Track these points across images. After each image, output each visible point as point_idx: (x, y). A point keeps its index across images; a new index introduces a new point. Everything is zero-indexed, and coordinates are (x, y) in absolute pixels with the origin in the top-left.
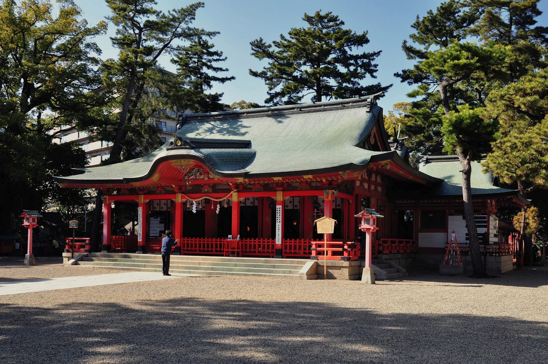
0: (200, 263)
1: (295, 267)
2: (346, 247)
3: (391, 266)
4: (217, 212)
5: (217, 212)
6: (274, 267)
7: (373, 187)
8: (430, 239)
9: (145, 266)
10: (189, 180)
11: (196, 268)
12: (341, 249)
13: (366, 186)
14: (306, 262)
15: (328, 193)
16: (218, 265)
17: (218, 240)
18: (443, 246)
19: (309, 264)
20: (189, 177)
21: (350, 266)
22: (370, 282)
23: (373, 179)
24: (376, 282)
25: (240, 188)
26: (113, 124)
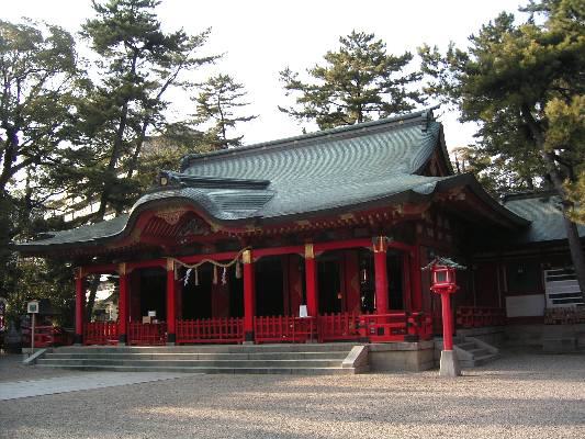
0: (198, 357)
1: (338, 356)
2: (411, 320)
3: (475, 346)
4: (197, 283)
5: (197, 283)
6: (305, 356)
7: (440, 236)
8: (524, 306)
9: (122, 364)
10: (184, 238)
11: (192, 364)
12: (403, 324)
13: (431, 233)
14: (352, 347)
15: (379, 241)
16: (225, 357)
17: (232, 320)
18: (542, 314)
19: (357, 350)
20: (184, 233)
21: (420, 350)
22: (453, 371)
23: (439, 224)
24: (463, 373)
25: (253, 242)
26: (557, 88)
